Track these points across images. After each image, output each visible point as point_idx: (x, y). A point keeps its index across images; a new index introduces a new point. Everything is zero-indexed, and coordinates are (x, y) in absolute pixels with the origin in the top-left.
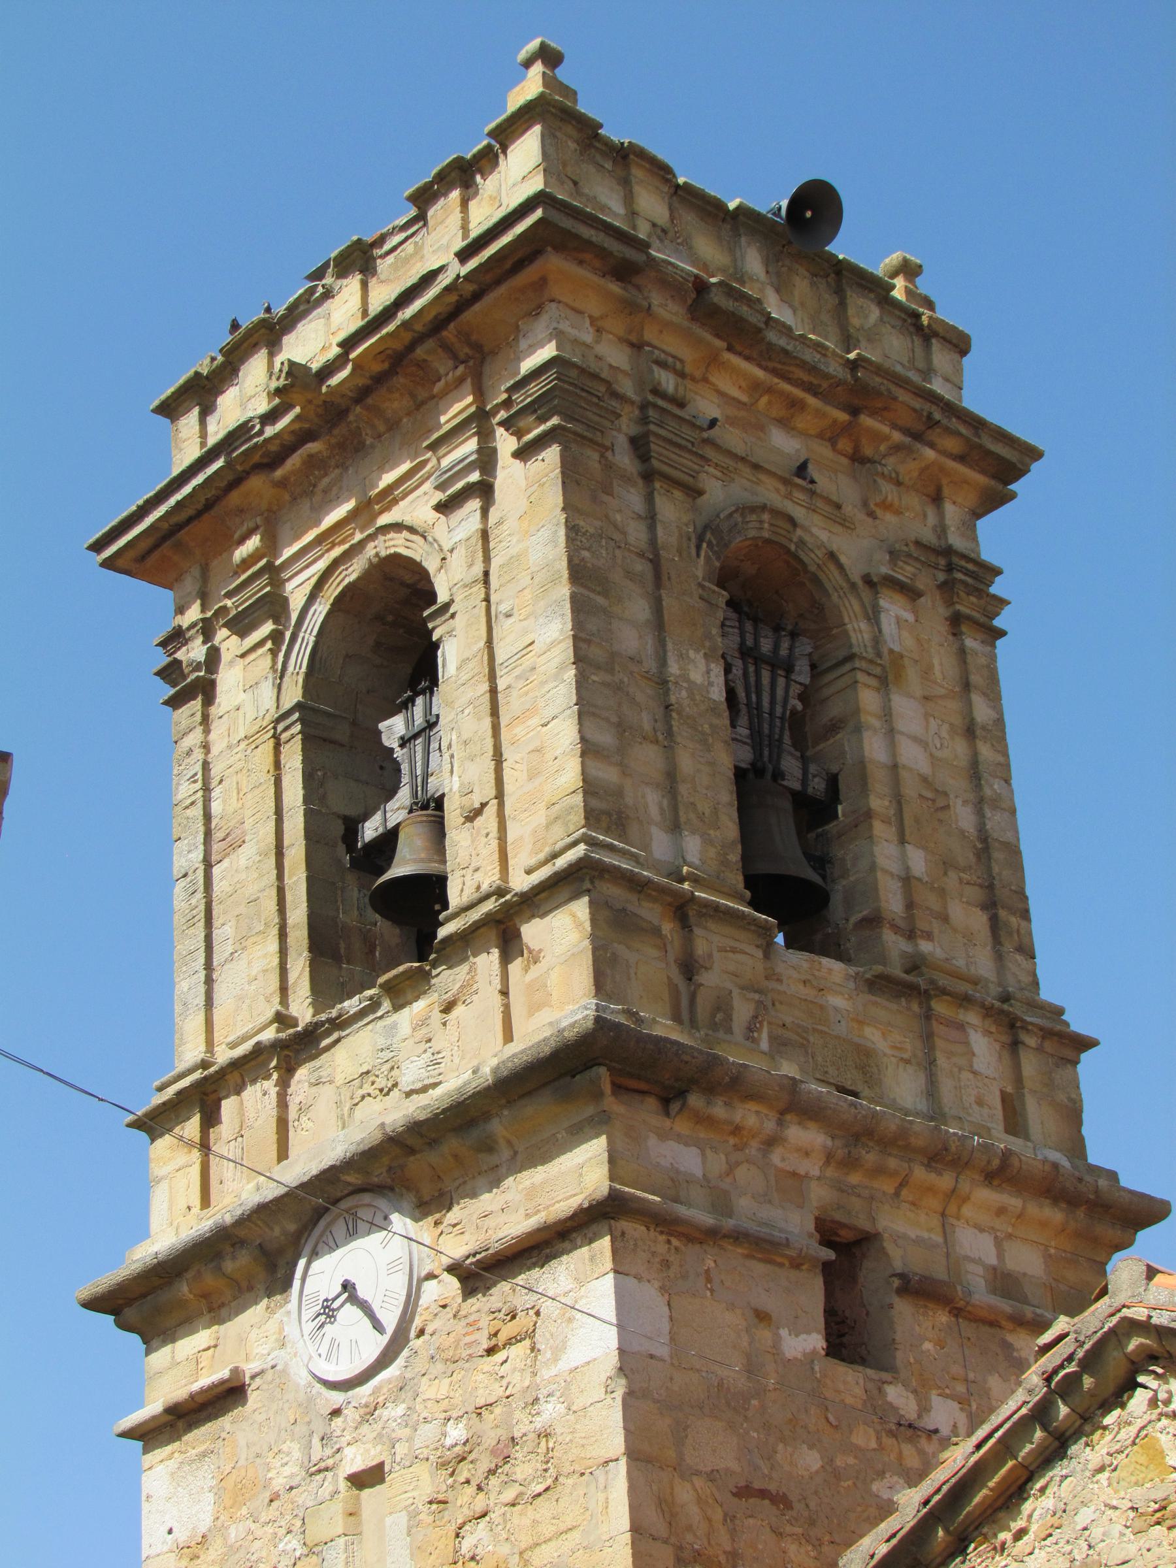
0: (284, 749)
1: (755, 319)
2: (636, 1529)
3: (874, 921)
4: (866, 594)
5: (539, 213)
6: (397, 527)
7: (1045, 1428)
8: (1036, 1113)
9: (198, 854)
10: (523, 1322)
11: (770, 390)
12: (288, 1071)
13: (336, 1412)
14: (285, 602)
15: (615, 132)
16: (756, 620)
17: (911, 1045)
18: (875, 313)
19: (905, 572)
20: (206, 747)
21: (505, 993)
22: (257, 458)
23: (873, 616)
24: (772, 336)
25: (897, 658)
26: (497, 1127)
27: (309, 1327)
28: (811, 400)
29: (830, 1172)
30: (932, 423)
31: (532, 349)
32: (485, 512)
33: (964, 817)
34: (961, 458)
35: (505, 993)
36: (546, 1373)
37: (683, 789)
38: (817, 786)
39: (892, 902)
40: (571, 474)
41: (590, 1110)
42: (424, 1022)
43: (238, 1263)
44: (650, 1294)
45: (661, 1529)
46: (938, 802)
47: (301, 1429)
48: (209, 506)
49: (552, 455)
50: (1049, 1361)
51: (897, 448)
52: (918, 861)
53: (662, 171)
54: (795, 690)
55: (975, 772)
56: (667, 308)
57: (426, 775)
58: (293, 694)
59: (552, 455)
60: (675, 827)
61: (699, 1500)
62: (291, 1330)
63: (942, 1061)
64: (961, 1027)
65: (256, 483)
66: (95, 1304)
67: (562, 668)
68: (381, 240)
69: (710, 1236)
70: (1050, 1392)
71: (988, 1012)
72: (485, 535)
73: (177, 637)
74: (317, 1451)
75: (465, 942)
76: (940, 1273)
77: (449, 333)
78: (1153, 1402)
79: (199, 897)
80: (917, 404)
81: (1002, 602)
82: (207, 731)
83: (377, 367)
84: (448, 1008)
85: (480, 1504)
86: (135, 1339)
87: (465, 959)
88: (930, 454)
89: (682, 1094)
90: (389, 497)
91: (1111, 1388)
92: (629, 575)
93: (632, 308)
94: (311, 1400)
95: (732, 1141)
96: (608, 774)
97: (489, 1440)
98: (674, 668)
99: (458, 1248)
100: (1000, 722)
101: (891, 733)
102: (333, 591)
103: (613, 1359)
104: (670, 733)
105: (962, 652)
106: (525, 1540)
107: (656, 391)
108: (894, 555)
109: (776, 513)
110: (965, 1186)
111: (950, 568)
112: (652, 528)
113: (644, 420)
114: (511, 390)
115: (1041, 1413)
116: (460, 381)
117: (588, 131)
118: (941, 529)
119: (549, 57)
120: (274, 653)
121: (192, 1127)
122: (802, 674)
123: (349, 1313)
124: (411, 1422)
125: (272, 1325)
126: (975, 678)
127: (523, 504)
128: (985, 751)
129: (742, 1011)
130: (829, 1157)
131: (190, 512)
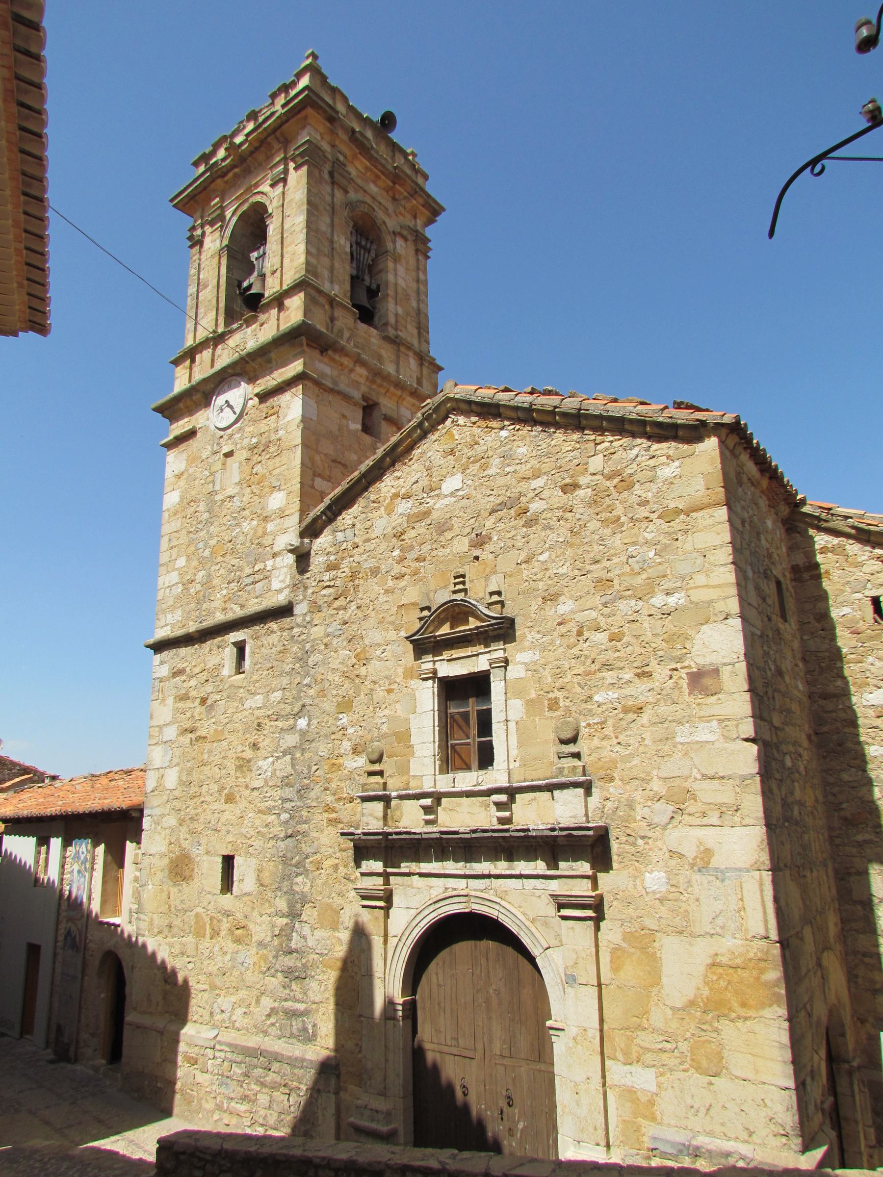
0: (222, 259)
1: (369, 146)
2: (302, 464)
3: (386, 324)
4: (393, 236)
5: (306, 92)
6: (259, 193)
7: (421, 429)
8: (425, 383)
9: (195, 289)
10: (276, 409)
11: (371, 170)
12: (215, 346)
13: (221, 437)
14: (225, 217)
15: (333, 82)
16: (361, 235)
17: (393, 357)
18: (403, 160)
19: (405, 233)
20: (200, 259)
21: (278, 320)
22: (219, 173)
23: (394, 242)
24: (373, 152)
25: (400, 256)
26: (273, 355)
27: (215, 414)
28: (383, 177)
29: (368, 383)
30: (416, 192)
31: (302, 138)
32: (284, 187)
33: (414, 304)
34: (423, 206)
35: (278, 320)
36: (281, 423)
37: (335, 272)
38: (374, 286)
39: (392, 319)
40: (310, 174)
41: (299, 350)
42: (255, 330)
43: (197, 397)
44: (312, 402)
45: (309, 465)
46: (407, 298)
47: (211, 442)
48: (205, 189)
49: (305, 169)
50: (424, 410)
51: (405, 198)
52: (400, 311)
53: (345, 99)
54: (370, 258)
55: (418, 292)
56: (344, 137)
57: (262, 267)
58: (226, 242)
59: (305, 169)
60: (332, 282)
61: (322, 461)
62: (211, 415)
63: (401, 363)
64: (407, 355)
65: (219, 181)
66: (155, 410)
67: (302, 229)
68: (261, 110)
69: (331, 391)
70: (424, 419)
71: (415, 353)
72: (283, 193)
73: (193, 228)
74: (216, 448)
75: (268, 306)
76: (395, 415)
77: (278, 133)
78: (453, 422)
79: (195, 302)
80: (412, 184)
81: (430, 249)
82: (200, 255)
83: (256, 144)
84: (262, 325)
85: (260, 459)
86: (167, 421)
87: (267, 311)
88: (414, 202)
89: (326, 350)
90: (257, 185)
91: (441, 418)
92: (325, 209)
93: (332, 132)
94: (215, 434)
96: (313, 261)
97: (263, 442)
98: (336, 238)
99: (257, 390)
100: (426, 280)
101: (396, 275)
102: (239, 213)
103: (300, 418)
104: (333, 256)
105: (418, 260)
106: (271, 468)
107: (338, 159)
108: (401, 227)
109: (369, 205)
110: (404, 395)
111: (417, 236)
112: (333, 198)
113: (333, 167)
114: (295, 150)
115: (420, 425)
116: (280, 149)
117: (324, 79)
118: (416, 225)
119: (314, 56)
120: (221, 231)
121: (188, 362)
122: (373, 254)
123: (228, 410)
124: (242, 439)
125: (206, 414)
126: (421, 267)
127: (295, 183)
128: (422, 287)
129: (346, 335)
130: (367, 378)
131: (199, 190)
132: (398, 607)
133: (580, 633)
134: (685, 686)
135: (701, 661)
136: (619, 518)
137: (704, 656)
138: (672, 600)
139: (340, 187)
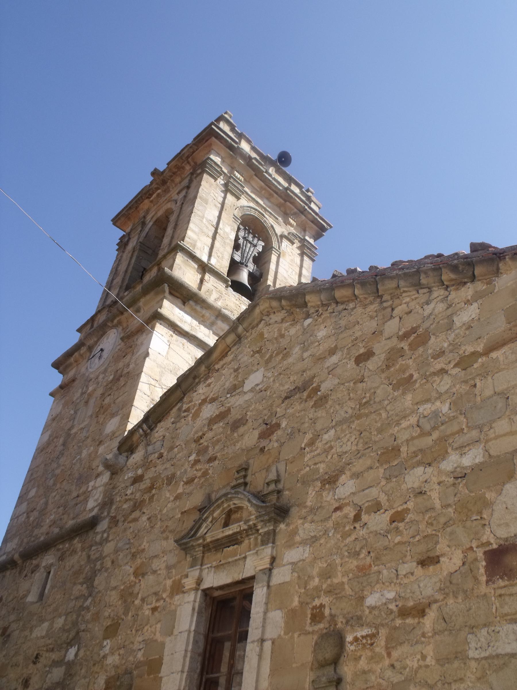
11: (265, 189)
28: (275, 195)
89: (189, 300)
95: (202, 319)
132: (182, 513)
133: (357, 518)
134: (482, 571)
135: (503, 533)
136: (411, 376)
137: (507, 525)
138: (467, 461)
139: (233, 194)
